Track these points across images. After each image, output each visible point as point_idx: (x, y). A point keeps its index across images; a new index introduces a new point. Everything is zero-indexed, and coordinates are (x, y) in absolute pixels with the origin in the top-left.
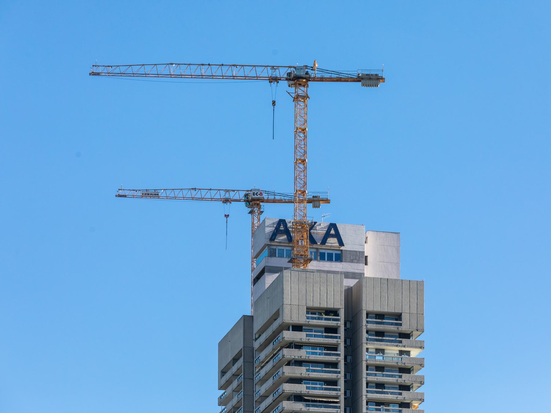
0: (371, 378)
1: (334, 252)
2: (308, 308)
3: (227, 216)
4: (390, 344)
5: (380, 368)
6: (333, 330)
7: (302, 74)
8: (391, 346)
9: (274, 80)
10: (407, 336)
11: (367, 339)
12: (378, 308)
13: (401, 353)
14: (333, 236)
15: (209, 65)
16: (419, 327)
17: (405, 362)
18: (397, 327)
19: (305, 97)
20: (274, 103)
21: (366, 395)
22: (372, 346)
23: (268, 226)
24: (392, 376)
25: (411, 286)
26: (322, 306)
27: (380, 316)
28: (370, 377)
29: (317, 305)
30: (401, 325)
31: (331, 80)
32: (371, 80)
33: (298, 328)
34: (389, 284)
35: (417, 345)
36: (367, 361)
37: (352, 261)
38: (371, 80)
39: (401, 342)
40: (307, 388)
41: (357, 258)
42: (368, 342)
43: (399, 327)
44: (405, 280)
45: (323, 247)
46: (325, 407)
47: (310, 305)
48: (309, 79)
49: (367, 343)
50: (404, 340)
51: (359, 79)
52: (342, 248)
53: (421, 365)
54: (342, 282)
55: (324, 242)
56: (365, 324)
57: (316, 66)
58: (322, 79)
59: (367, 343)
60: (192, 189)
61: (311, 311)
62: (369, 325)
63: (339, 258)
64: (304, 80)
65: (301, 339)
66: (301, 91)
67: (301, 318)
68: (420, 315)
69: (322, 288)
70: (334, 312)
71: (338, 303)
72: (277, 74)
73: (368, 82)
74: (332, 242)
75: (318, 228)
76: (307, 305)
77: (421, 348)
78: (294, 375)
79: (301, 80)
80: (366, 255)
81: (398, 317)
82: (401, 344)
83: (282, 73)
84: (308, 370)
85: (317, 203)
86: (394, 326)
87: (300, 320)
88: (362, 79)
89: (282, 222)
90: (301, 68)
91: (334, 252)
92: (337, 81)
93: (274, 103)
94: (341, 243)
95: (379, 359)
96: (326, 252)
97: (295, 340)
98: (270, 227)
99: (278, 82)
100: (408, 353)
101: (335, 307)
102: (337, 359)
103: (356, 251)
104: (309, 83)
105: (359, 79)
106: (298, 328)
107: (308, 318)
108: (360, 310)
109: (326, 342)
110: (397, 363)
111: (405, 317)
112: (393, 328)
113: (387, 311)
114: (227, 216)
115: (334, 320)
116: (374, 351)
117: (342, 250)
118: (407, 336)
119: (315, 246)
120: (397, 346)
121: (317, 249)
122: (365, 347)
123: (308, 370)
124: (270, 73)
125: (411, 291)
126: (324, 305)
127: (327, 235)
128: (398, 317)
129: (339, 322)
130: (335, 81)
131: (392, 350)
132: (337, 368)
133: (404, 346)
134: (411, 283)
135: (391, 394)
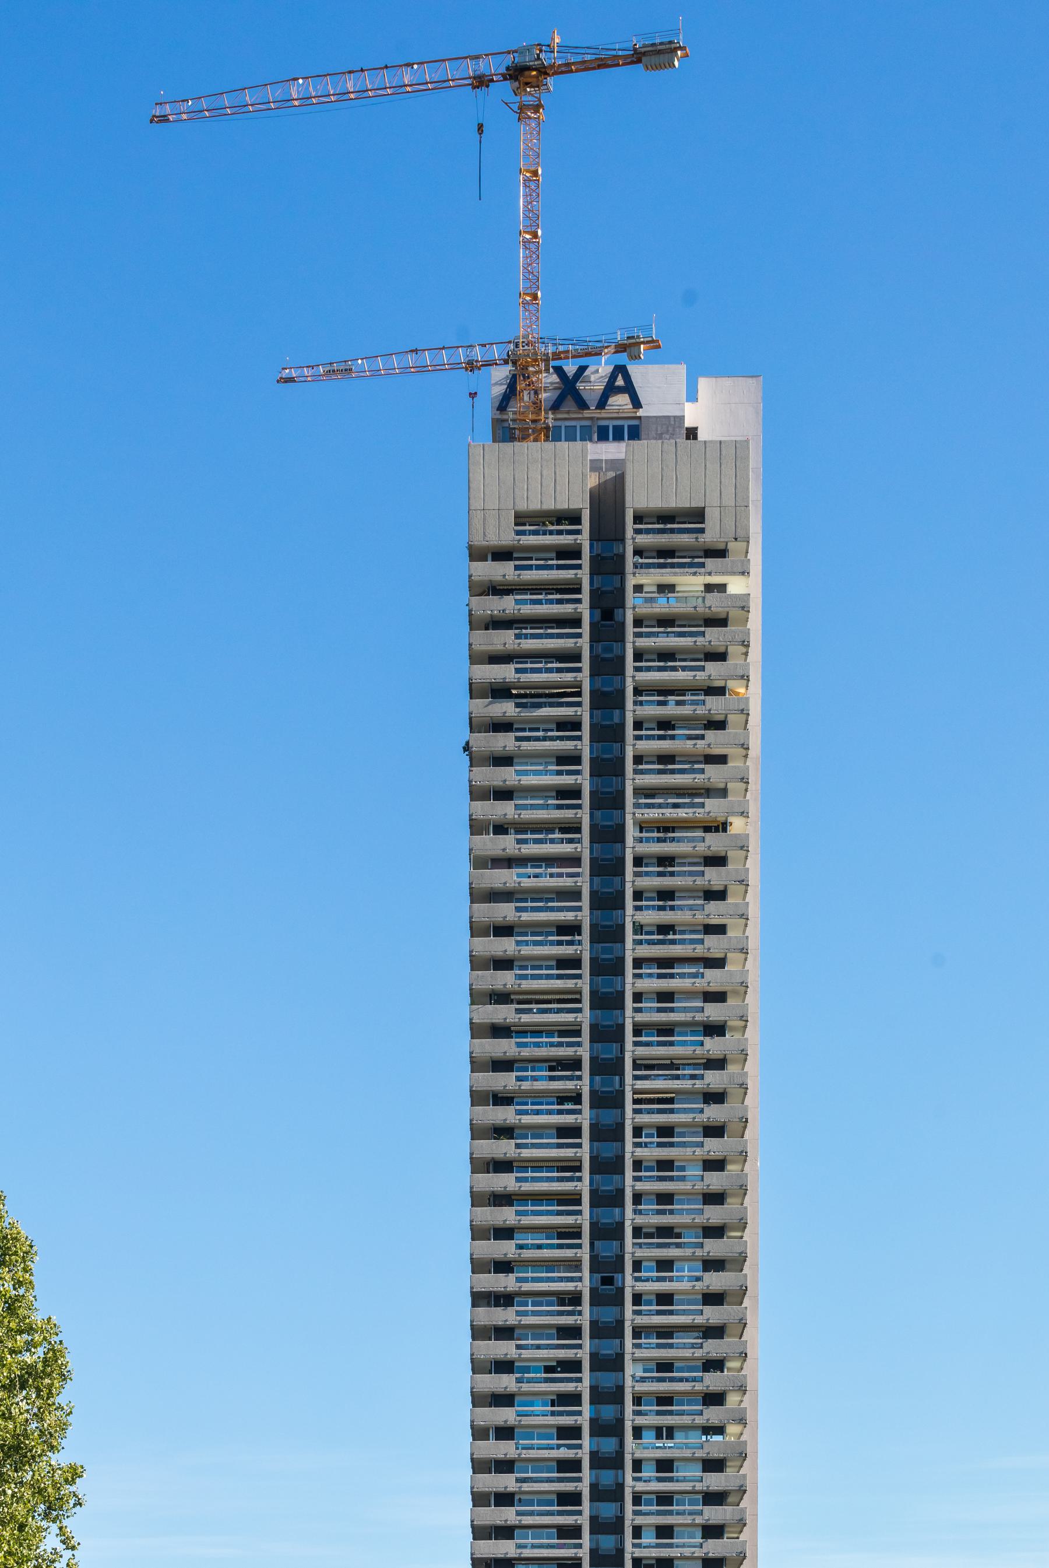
0: (643, 643)
1: (626, 424)
3: (473, 395)
4: (682, 570)
5: (666, 622)
6: (571, 553)
7: (528, 59)
8: (683, 574)
9: (481, 82)
10: (720, 553)
11: (636, 566)
13: (709, 588)
14: (620, 390)
15: (362, 70)
16: (741, 533)
17: (715, 604)
18: (695, 535)
19: (537, 108)
20: (480, 127)
21: (633, 677)
22: (650, 579)
23: (496, 384)
25: (724, 453)
26: (545, 507)
27: (666, 517)
28: (641, 639)
29: (535, 505)
31: (586, 67)
32: (654, 55)
34: (679, 452)
35: (735, 570)
36: (634, 608)
38: (654, 55)
39: (703, 565)
40: (517, 671)
41: (670, 429)
42: (637, 571)
43: (699, 535)
44: (711, 442)
45: (603, 414)
46: (551, 705)
47: (522, 506)
48: (544, 71)
49: (634, 574)
50: (710, 563)
51: (637, 57)
52: (641, 413)
53: (743, 608)
54: (584, 453)
55: (602, 404)
57: (557, 40)
58: (566, 69)
59: (634, 574)
60: (412, 351)
61: (521, 519)
62: (639, 536)
64: (534, 73)
65: (504, 576)
66: (529, 96)
69: (545, 473)
70: (574, 518)
72: (483, 67)
73: (655, 59)
75: (592, 378)
76: (516, 508)
77: (743, 573)
78: (490, 648)
79: (527, 73)
80: (688, 423)
81: (698, 515)
82: (702, 570)
83: (493, 66)
84: (518, 636)
85: (634, 350)
87: (502, 538)
88: (644, 54)
90: (528, 49)
91: (626, 424)
92: (599, 67)
93: (480, 127)
94: (637, 403)
95: (663, 606)
96: (611, 424)
97: (493, 578)
98: (501, 384)
99: (488, 86)
100: (722, 588)
101: (571, 507)
102: (576, 609)
103: (668, 417)
104: (550, 81)
105: (637, 57)
107: (518, 533)
109: (553, 577)
110: (695, 607)
111: (712, 516)
112: (685, 539)
113: (674, 505)
114: (473, 395)
116: (655, 589)
117: (640, 418)
119: (586, 414)
120: (695, 574)
121: (591, 419)
122: (631, 581)
123: (518, 636)
124: (470, 69)
125: (723, 462)
126: (549, 505)
127: (610, 389)
128: (698, 515)
129: (579, 537)
130: (594, 69)
131: (690, 583)
133: (710, 574)
134: (723, 445)
135: (683, 670)
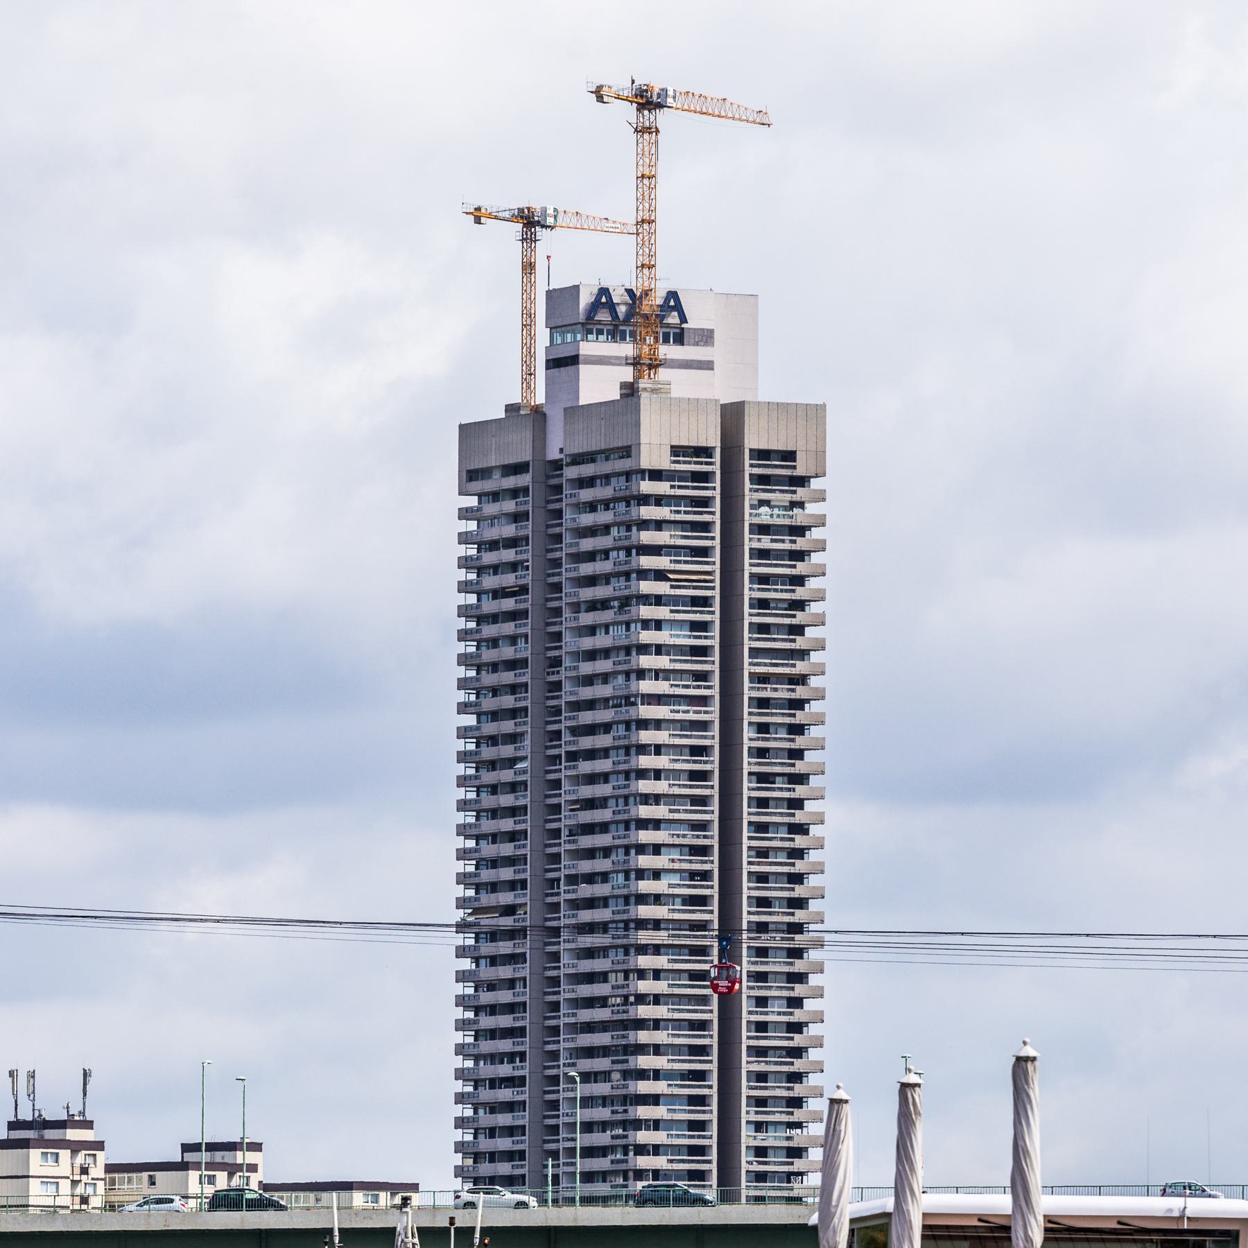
2: (672, 447)
12: (763, 446)
17: (799, 516)
24: (783, 541)
30: (795, 467)
33: (656, 475)
37: (697, 344)
46: (695, 588)
56: (749, 468)
61: (676, 451)
63: (680, 339)
67: (663, 461)
68: (820, 455)
70: (705, 452)
71: (712, 438)
74: (673, 319)
86: (786, 471)
89: (604, 291)
94: (683, 319)
106: (656, 475)
108: (741, 447)
115: (707, 463)
118: (802, 481)
128: (789, 456)
132: (709, 532)
